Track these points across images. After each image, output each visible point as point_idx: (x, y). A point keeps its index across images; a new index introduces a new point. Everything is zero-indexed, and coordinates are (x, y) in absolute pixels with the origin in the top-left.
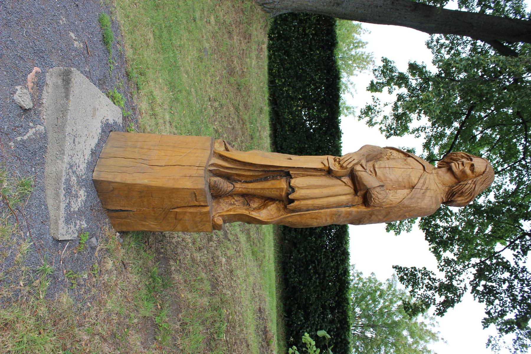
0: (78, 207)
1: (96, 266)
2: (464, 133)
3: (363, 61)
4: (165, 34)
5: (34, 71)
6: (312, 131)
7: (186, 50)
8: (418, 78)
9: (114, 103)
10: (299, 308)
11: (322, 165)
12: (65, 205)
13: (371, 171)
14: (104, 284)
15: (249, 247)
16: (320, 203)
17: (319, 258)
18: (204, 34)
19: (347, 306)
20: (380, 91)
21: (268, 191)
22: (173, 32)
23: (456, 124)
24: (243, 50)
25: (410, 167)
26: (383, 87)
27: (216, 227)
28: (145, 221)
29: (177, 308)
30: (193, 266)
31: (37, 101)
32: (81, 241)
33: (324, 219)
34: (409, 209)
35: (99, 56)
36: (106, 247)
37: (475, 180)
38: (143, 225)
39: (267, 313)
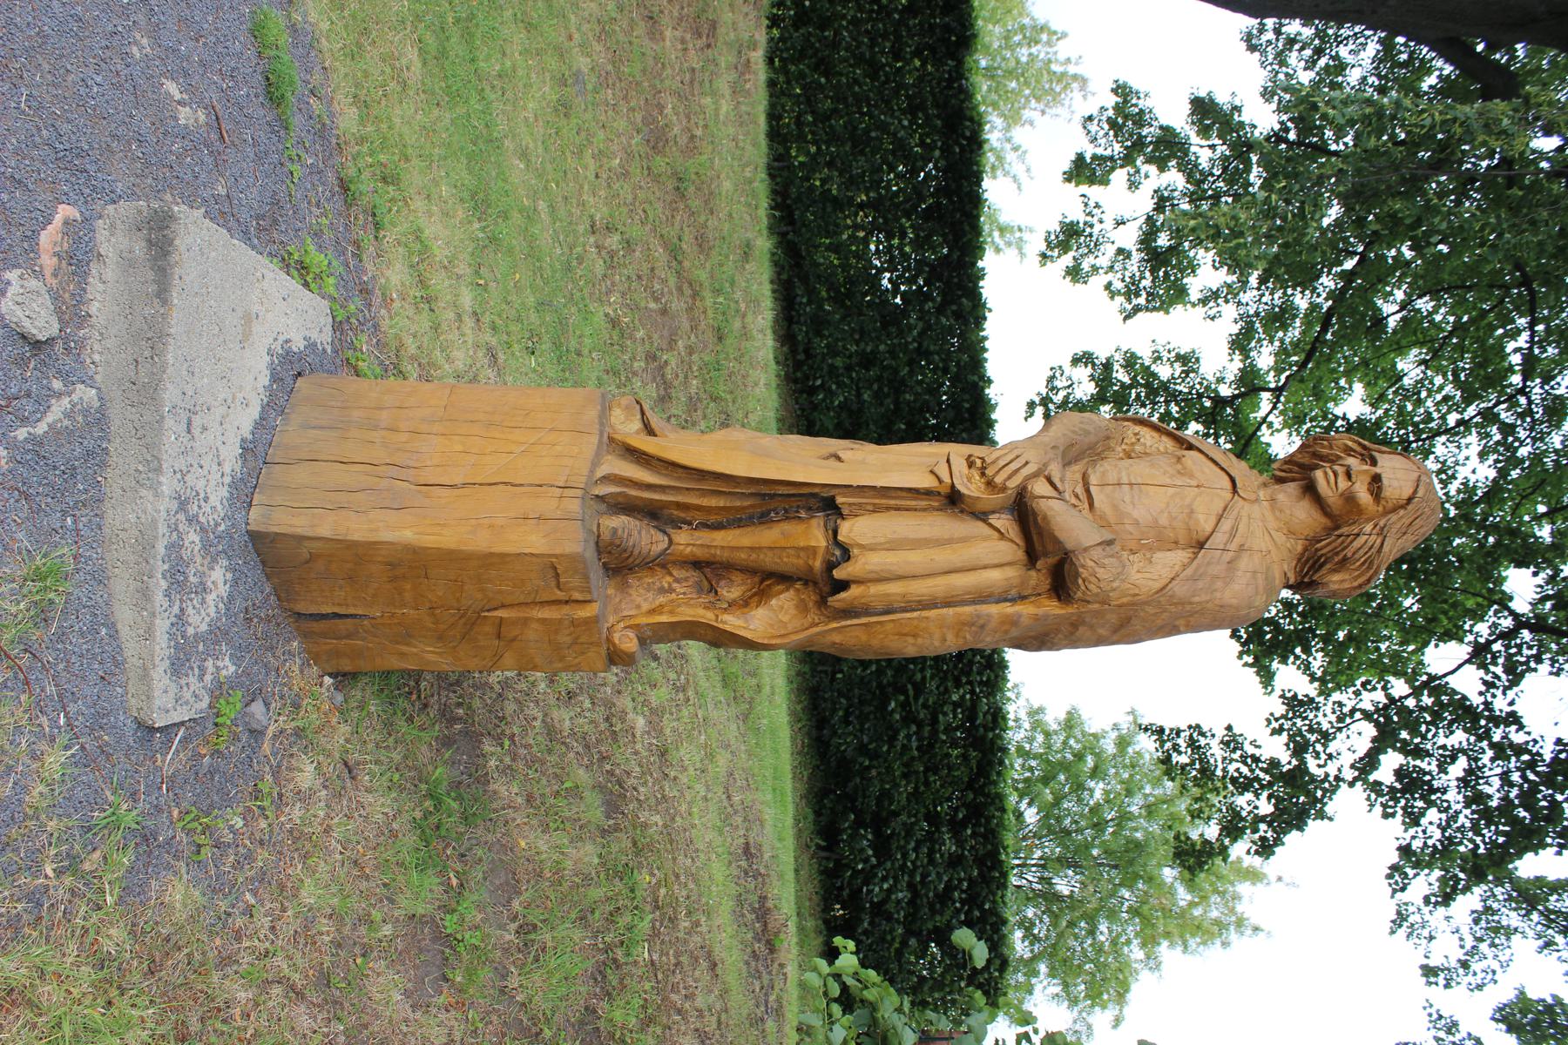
0: (207, 619)
1: (267, 783)
2: (1351, 317)
3: (1051, 84)
4: (456, 46)
5: (58, 219)
6: (898, 300)
7: (521, 85)
8: (1217, 141)
9: (306, 285)
10: (859, 823)
11: (932, 477)
12: (168, 623)
13: (1077, 496)
14: (291, 831)
15: (714, 662)
16: (925, 591)
17: (918, 676)
18: (573, 30)
19: (1001, 818)
20: (1104, 182)
21: (770, 554)
22: (479, 35)
23: (1327, 282)
24: (693, 70)
25: (1194, 483)
26: (1113, 169)
27: (616, 659)
28: (408, 644)
29: (507, 883)
30: (550, 751)
31: (72, 312)
32: (219, 720)
33: (937, 636)
34: (1188, 607)
35: (255, 143)
36: (293, 724)
37: (1382, 523)
38: (402, 655)
39: (766, 856)
